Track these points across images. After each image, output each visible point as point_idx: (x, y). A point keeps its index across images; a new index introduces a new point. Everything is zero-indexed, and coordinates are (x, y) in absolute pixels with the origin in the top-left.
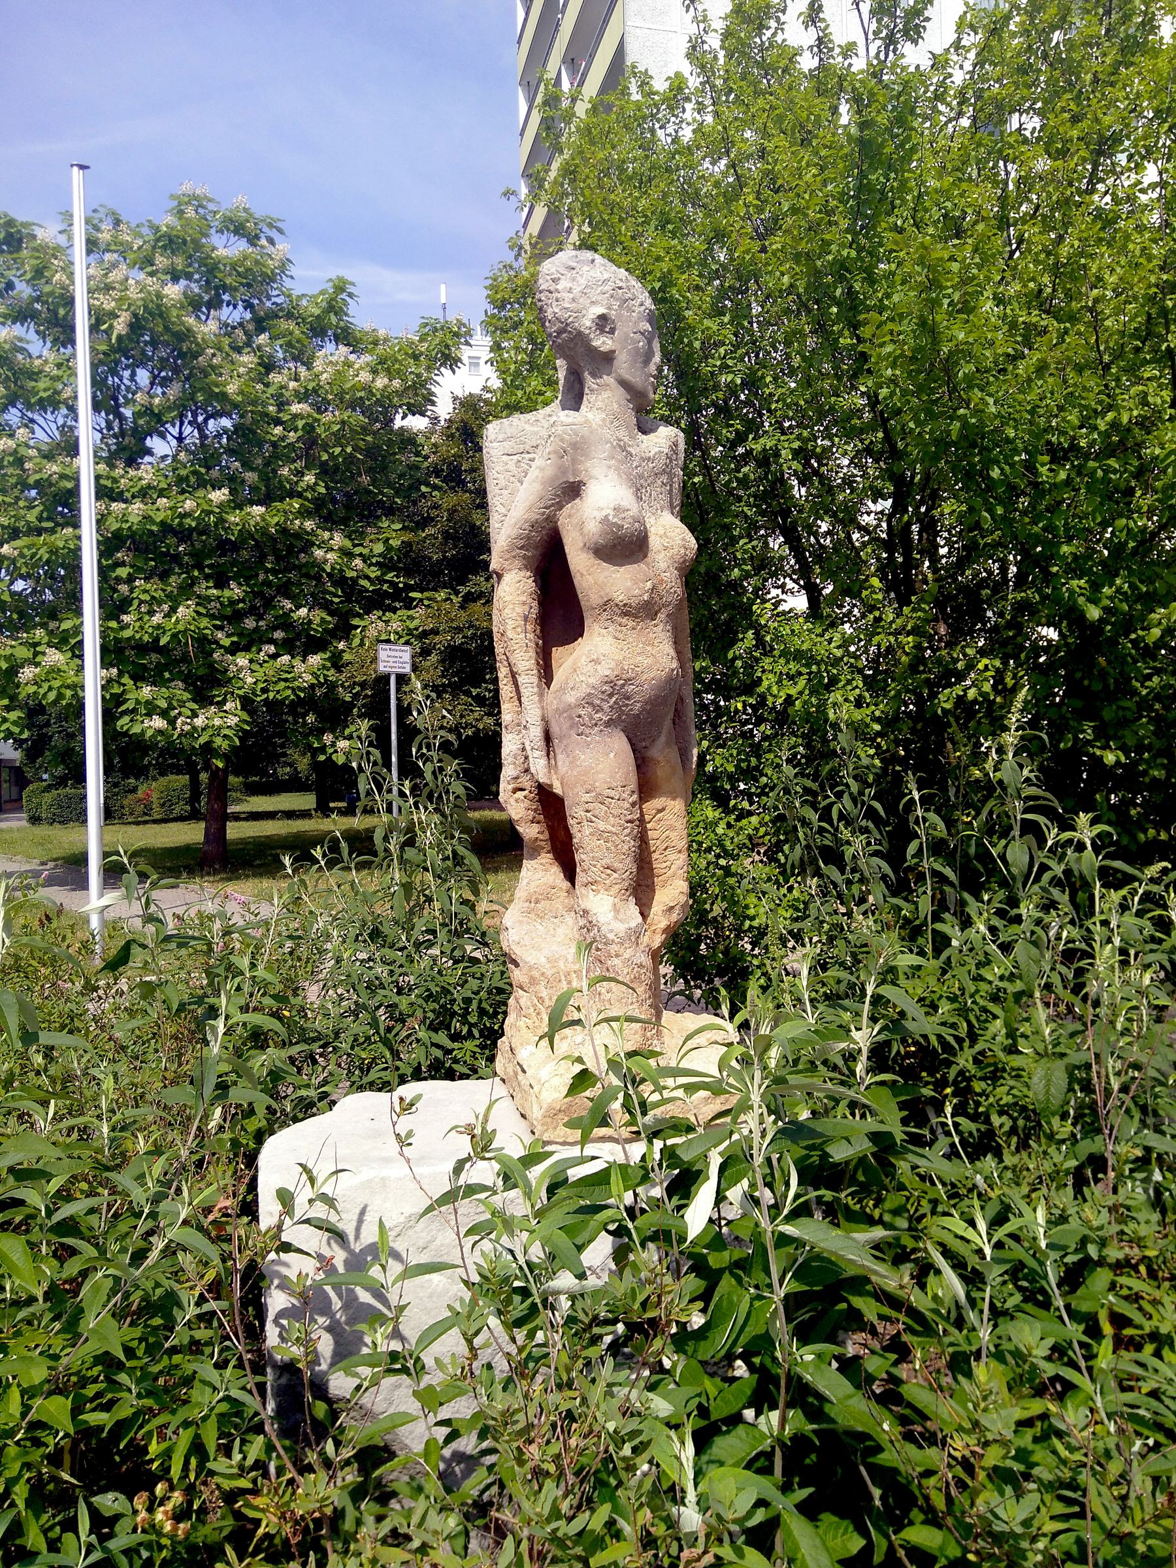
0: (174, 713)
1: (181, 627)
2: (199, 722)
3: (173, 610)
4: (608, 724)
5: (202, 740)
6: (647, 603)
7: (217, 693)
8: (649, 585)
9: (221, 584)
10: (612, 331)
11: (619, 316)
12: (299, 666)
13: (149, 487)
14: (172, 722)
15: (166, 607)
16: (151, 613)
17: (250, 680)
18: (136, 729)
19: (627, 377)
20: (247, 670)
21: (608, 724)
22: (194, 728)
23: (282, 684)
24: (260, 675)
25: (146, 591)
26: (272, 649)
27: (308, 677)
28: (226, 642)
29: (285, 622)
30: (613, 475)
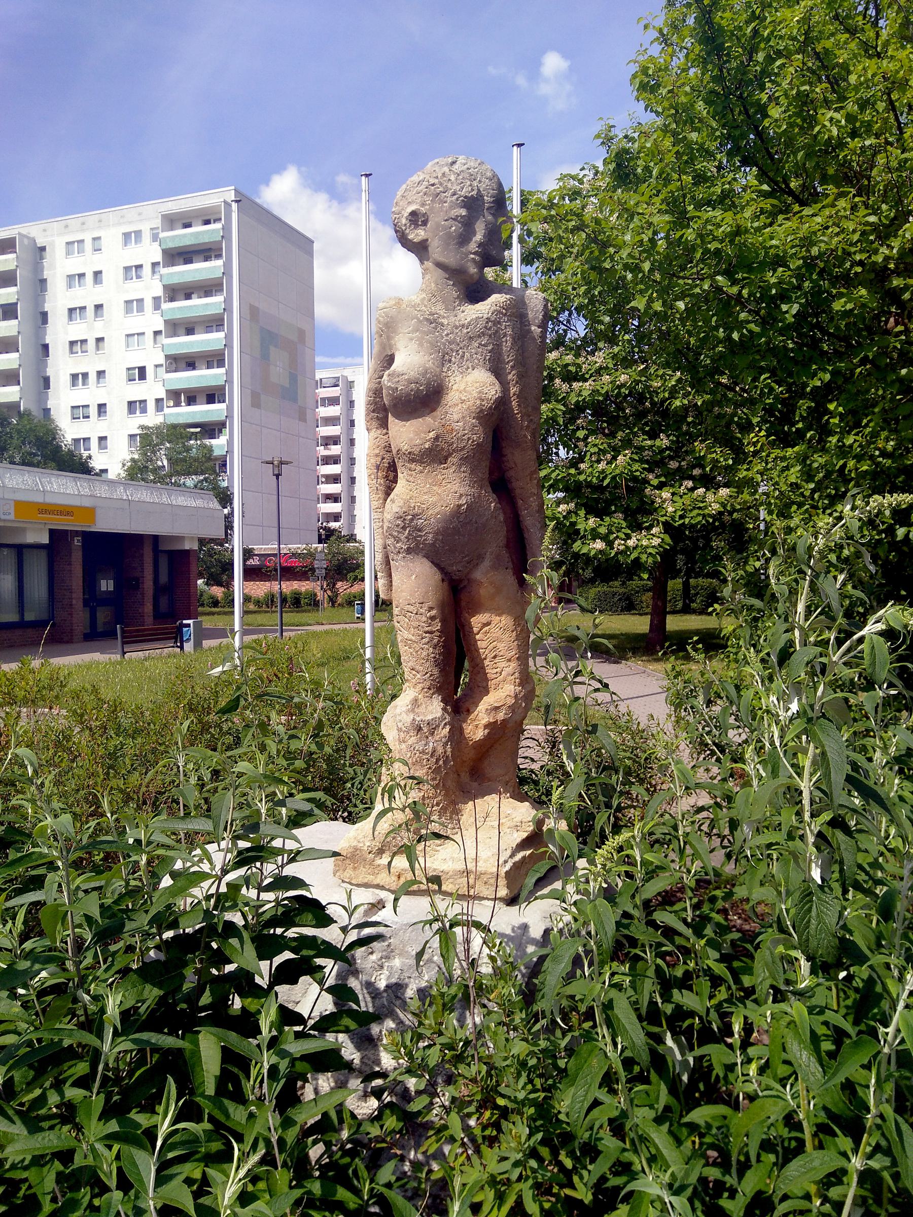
0: (612, 537)
1: (618, 472)
2: (630, 543)
3: (615, 458)
4: (409, 551)
5: (633, 557)
6: (430, 450)
7: (646, 521)
8: (432, 435)
9: (653, 435)
10: (425, 223)
11: (432, 209)
12: (710, 497)
13: (601, 368)
14: (610, 544)
15: (609, 456)
16: (598, 461)
17: (670, 509)
18: (584, 551)
19: (442, 259)
20: (669, 502)
21: (409, 551)
22: (627, 548)
23: (696, 512)
24: (679, 505)
25: (595, 445)
26: (690, 484)
27: (716, 506)
28: (655, 482)
29: (699, 462)
30: (414, 345)
